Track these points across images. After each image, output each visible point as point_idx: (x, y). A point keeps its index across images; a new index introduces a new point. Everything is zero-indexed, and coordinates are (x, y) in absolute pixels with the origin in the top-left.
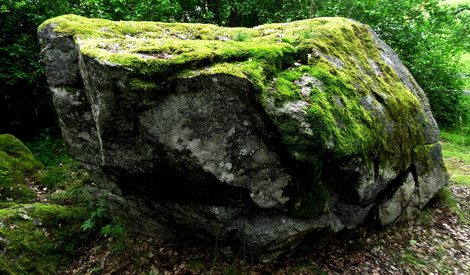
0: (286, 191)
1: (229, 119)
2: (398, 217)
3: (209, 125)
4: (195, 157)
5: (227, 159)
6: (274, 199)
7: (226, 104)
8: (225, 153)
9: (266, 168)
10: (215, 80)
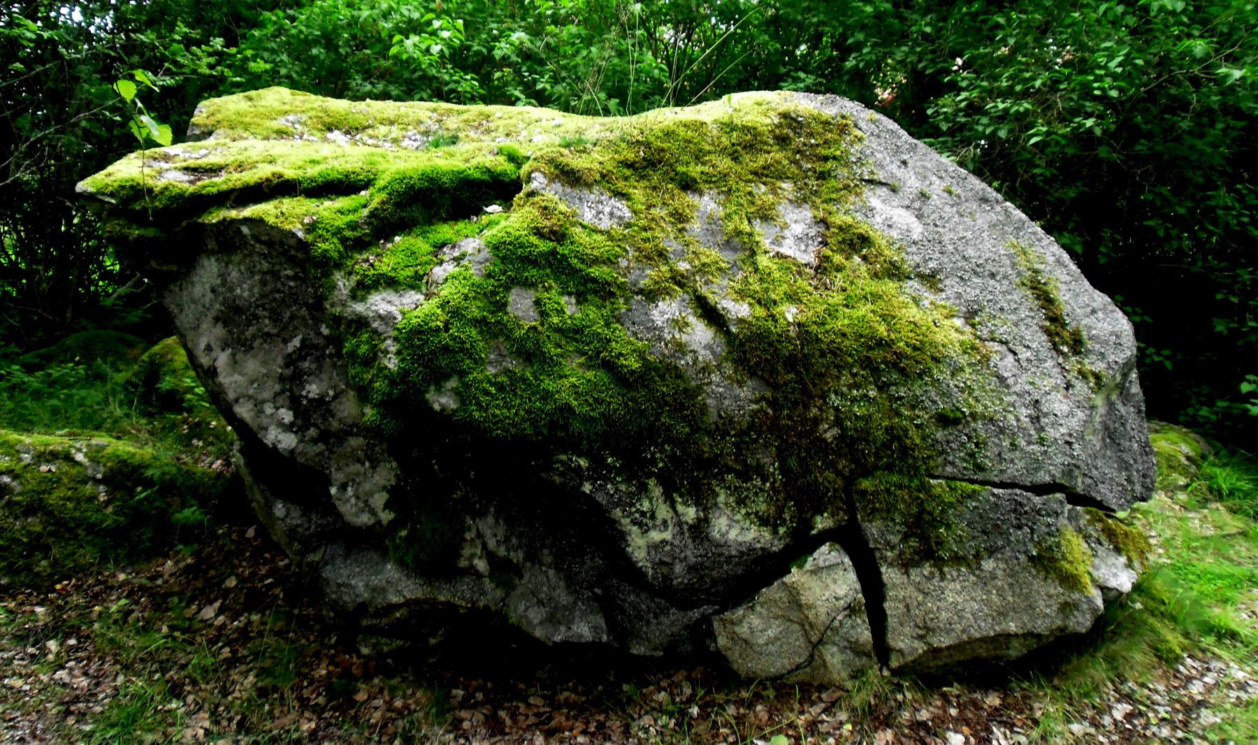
0: (396, 499)
1: (292, 317)
2: (798, 667)
3: (249, 324)
4: (221, 385)
5: (280, 400)
6: (372, 512)
7: (284, 285)
8: (277, 387)
9: (357, 435)
10: (245, 230)
